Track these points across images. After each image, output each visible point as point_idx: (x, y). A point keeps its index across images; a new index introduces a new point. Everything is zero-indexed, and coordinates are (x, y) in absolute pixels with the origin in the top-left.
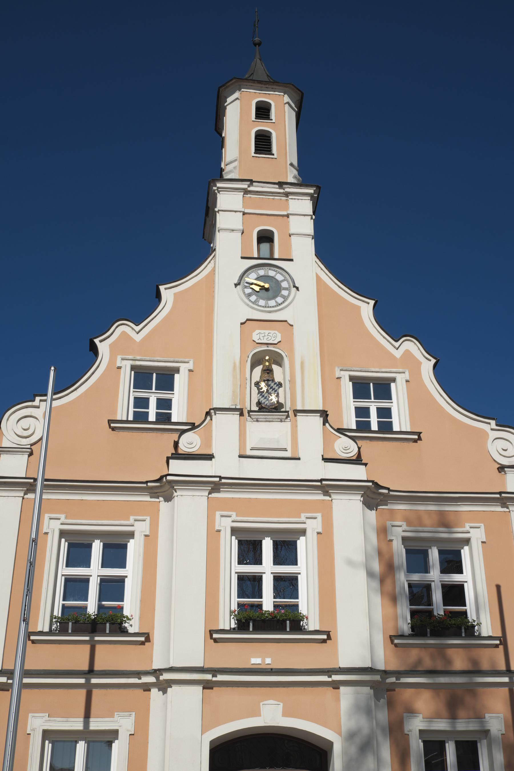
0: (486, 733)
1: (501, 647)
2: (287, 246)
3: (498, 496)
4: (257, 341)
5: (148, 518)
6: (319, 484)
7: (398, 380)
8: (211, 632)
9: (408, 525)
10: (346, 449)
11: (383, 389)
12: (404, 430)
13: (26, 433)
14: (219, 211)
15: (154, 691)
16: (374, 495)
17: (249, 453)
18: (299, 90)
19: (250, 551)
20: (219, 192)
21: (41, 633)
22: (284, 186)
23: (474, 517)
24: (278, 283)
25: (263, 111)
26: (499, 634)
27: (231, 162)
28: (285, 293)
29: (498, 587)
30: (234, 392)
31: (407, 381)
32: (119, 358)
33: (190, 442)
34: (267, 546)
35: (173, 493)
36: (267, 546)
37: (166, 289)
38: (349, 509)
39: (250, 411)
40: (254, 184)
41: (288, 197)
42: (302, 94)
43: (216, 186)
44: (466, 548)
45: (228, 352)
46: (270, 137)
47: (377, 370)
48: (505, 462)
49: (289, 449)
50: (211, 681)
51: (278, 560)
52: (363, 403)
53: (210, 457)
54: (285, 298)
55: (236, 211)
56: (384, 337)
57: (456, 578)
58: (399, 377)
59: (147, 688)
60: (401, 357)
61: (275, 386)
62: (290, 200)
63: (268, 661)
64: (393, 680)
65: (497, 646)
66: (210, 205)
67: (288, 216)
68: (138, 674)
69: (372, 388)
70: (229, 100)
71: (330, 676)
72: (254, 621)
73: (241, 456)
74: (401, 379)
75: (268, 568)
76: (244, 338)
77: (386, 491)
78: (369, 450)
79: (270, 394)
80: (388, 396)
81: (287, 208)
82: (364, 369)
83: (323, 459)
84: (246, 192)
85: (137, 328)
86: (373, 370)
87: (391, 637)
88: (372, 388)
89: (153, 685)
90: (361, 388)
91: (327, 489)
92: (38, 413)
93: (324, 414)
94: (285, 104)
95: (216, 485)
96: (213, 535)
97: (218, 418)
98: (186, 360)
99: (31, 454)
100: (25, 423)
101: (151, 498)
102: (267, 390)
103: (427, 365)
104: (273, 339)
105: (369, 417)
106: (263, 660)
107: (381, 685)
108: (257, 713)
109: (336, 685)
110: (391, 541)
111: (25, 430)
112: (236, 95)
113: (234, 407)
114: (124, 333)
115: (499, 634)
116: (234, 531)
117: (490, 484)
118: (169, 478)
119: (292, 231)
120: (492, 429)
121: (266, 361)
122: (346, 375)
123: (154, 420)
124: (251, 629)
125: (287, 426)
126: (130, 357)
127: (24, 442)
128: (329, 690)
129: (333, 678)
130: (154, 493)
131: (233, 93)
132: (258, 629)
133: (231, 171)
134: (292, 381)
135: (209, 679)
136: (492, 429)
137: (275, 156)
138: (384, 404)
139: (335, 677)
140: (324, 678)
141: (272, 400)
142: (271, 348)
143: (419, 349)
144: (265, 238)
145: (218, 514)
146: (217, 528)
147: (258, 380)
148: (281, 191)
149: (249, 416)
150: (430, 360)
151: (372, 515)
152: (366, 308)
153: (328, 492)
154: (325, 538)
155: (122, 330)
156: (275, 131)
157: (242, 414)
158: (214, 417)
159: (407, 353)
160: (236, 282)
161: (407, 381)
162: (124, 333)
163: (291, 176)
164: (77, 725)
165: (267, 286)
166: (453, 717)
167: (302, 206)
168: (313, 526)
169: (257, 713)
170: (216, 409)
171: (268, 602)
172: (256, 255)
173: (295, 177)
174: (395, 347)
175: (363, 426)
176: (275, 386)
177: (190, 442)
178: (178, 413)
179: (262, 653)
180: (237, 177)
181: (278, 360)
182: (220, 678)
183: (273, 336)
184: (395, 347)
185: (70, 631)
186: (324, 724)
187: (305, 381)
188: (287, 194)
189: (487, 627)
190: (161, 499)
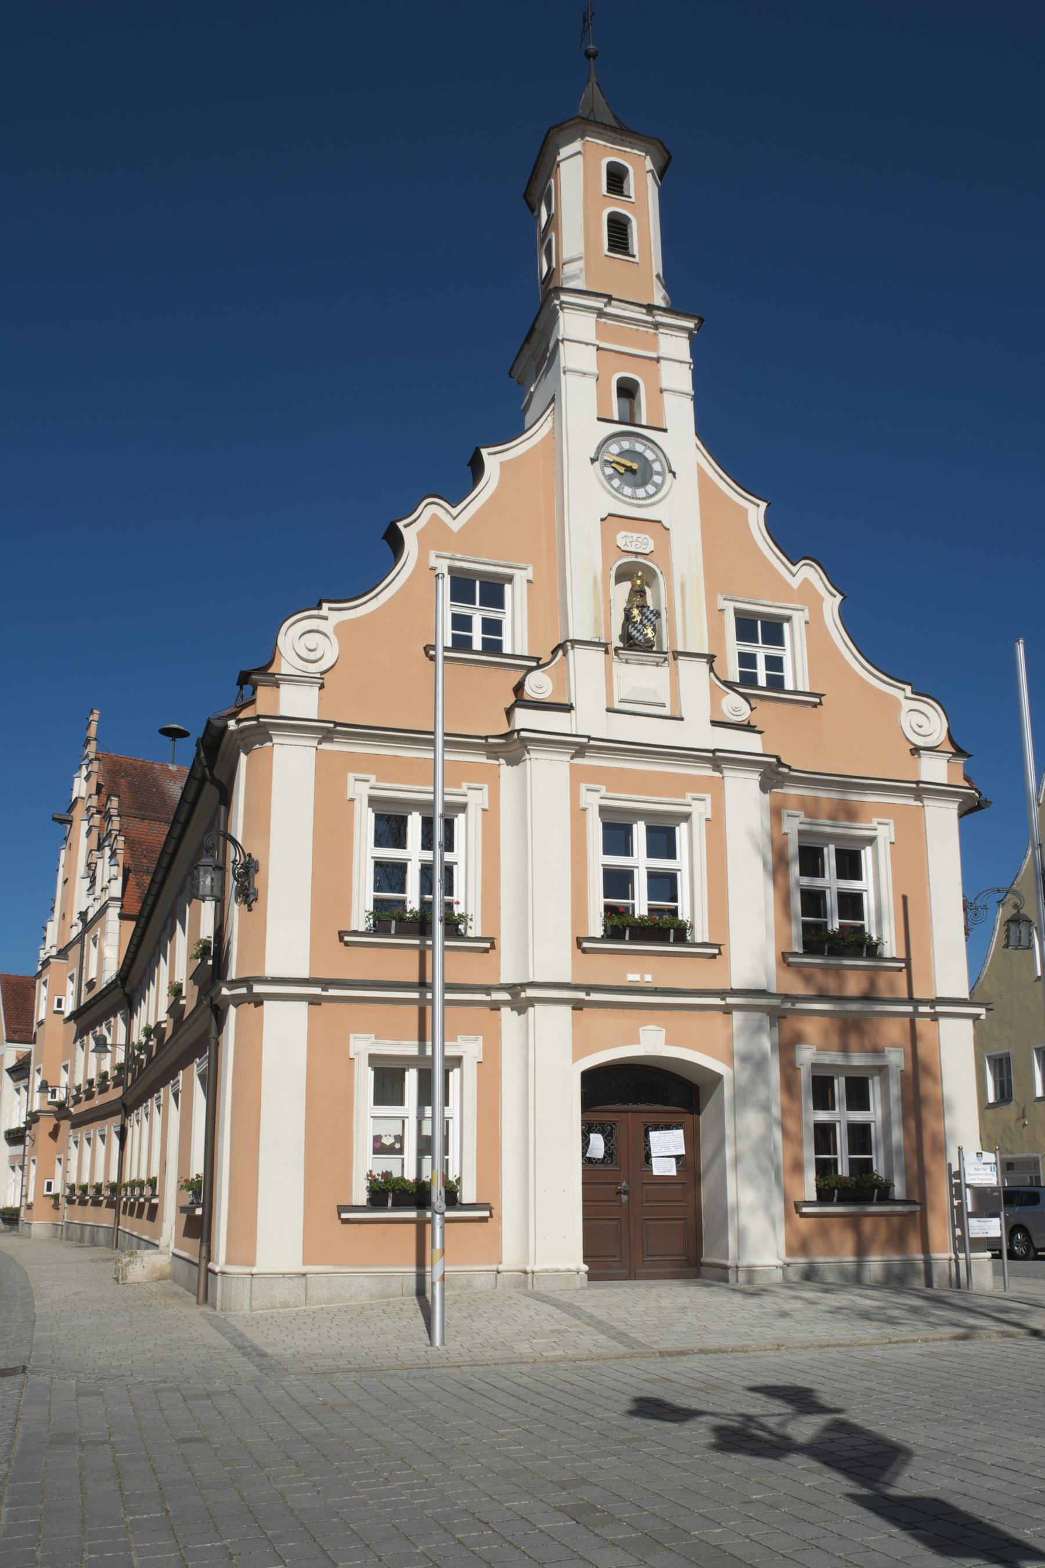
0: (882, 1070)
1: (904, 970)
2: (657, 407)
3: (914, 786)
5: (486, 787)
6: (710, 755)
7: (517, 580)
9: (806, 816)
10: (736, 709)
11: (773, 632)
13: (312, 656)
14: (564, 340)
15: (505, 1011)
16: (773, 774)
17: (617, 706)
18: (667, 151)
19: (617, 838)
20: (562, 309)
21: (355, 933)
22: (655, 312)
23: (884, 811)
24: (646, 463)
25: (616, 179)
26: (903, 956)
27: (573, 260)
28: (657, 479)
29: (905, 898)
30: (596, 619)
31: (529, 582)
32: (432, 554)
33: (539, 685)
34: (639, 832)
35: (524, 755)
36: (639, 832)
37: (489, 454)
38: (743, 791)
39: (617, 649)
40: (613, 302)
41: (657, 329)
42: (670, 158)
43: (558, 298)
44: (869, 849)
45: (585, 559)
46: (626, 226)
47: (770, 603)
48: (920, 742)
49: (668, 705)
50: (583, 1000)
52: (748, 648)
53: (568, 708)
54: (659, 487)
55: (587, 344)
56: (778, 557)
57: (853, 885)
58: (796, 616)
59: (496, 1006)
60: (800, 587)
61: (651, 616)
62: (660, 335)
63: (648, 978)
64: (788, 1005)
65: (900, 969)
66: (539, 326)
67: (658, 360)
68: (488, 989)
69: (761, 628)
70: (564, 152)
71: (723, 999)
72: (632, 928)
73: (608, 710)
74: (799, 618)
75: (640, 861)
76: (607, 540)
77: (786, 770)
78: (767, 714)
79: (645, 626)
80: (499, 603)
81: (655, 347)
82: (753, 601)
83: (712, 722)
84: (601, 314)
85: (454, 511)
86: (765, 602)
87: (783, 954)
88: (761, 628)
89: (505, 1003)
91: (719, 762)
92: (327, 627)
93: (711, 659)
94: (648, 172)
95: (581, 747)
96: (578, 814)
97: (578, 656)
98: (523, 565)
99: (322, 687)
100: (312, 640)
101: (488, 758)
103: (831, 603)
104: (644, 546)
105: (483, 639)
106: (642, 977)
107: (775, 1010)
108: (635, 1040)
109: (727, 1010)
111: (310, 650)
112: (576, 146)
113: (597, 640)
114: (435, 516)
115: (903, 956)
116: (373, 801)
117: (900, 769)
118: (523, 734)
119: (664, 386)
120: (906, 698)
121: (636, 575)
122: (730, 607)
123: (480, 649)
124: (627, 938)
125: (664, 672)
126: (448, 554)
127: (313, 668)
128: (719, 1016)
129: (727, 1000)
130: (493, 752)
131: (571, 141)
132: (635, 938)
133: (575, 277)
134: (671, 610)
135: (581, 998)
136: (906, 698)
138: (492, 614)
139: (730, 1000)
140: (717, 1001)
141: (646, 634)
142: (640, 560)
143: (821, 578)
144: (627, 390)
145: (583, 786)
146: (350, 796)
148: (649, 319)
149: (617, 654)
150: (835, 596)
151: (767, 797)
152: (756, 512)
153: (719, 766)
154: (716, 825)
155: (431, 511)
156: (635, 217)
157: (607, 652)
158: (570, 652)
159: (806, 582)
162: (435, 516)
163: (659, 297)
164: (411, 1048)
165: (635, 466)
166: (845, 1049)
167: (675, 346)
168: (701, 811)
169: (635, 1040)
170: (575, 642)
171: (641, 904)
173: (664, 298)
174: (791, 572)
175: (748, 680)
176: (651, 616)
177: (539, 685)
179: (641, 968)
180: (583, 287)
181: (650, 576)
182: (595, 997)
183: (640, 542)
184: (791, 572)
185: (393, 932)
187: (692, 614)
188: (657, 326)
189: (891, 947)
190: (502, 761)
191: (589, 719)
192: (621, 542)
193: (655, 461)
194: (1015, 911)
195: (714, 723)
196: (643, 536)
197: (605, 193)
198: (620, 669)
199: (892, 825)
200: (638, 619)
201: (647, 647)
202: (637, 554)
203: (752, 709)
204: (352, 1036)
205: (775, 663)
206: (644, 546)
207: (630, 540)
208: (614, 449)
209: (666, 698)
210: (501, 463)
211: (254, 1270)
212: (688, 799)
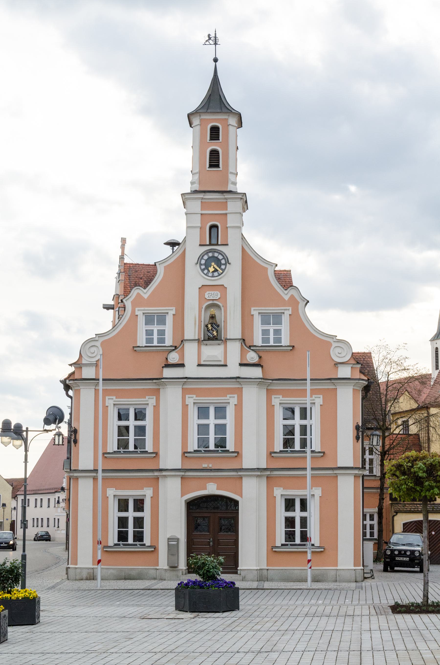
4: (207, 299)
8: (184, 453)
10: (252, 358)
13: (93, 355)
17: (202, 363)
21: (109, 453)
33: (174, 358)
49: (223, 360)
52: (266, 327)
63: (210, 466)
75: (212, 421)
96: (185, 407)
100: (93, 349)
102: (212, 329)
110: (188, 405)
114: (138, 294)
125: (222, 347)
147: (207, 323)
160: (196, 262)
161: (290, 315)
162: (138, 294)
168: (233, 400)
170: (185, 340)
172: (208, 243)
178: (169, 341)
183: (215, 295)
186: (235, 493)
191: (191, 370)
192: (206, 296)
193: (222, 259)
197: (208, 141)
198: (203, 348)
200: (210, 328)
201: (215, 338)
202: (213, 300)
206: (216, 296)
208: (206, 257)
210: (164, 267)
211: (338, 568)
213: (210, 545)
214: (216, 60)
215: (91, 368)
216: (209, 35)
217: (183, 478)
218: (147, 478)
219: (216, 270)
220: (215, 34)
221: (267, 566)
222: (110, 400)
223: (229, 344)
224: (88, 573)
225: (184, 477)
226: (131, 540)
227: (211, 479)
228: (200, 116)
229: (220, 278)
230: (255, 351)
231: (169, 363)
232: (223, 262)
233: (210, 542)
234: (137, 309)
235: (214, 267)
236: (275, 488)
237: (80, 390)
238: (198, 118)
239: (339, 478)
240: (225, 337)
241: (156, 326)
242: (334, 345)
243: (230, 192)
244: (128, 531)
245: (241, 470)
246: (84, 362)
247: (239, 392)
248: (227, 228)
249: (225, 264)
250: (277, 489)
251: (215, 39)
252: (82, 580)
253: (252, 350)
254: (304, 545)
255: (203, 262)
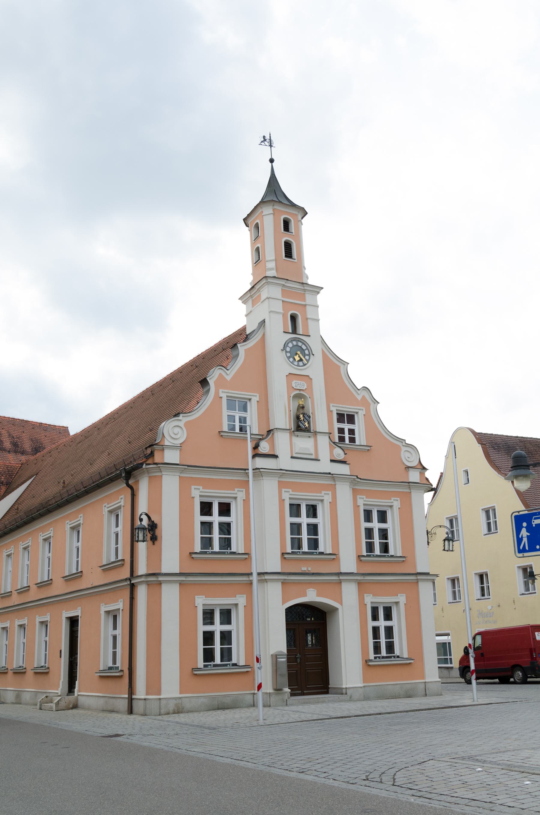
10: (339, 455)
11: (351, 419)
12: (362, 444)
17: (295, 455)
21: (196, 553)
33: (264, 447)
38: (344, 492)
51: (221, 514)
52: (341, 426)
58: (360, 412)
73: (292, 457)
74: (361, 413)
76: (290, 387)
90: (341, 418)
95: (282, 473)
100: (177, 430)
108: (305, 595)
110: (284, 500)
114: (220, 374)
118: (261, 470)
125: (312, 440)
133: (271, 269)
137: (296, 261)
142: (301, 392)
144: (293, 318)
145: (283, 490)
154: (333, 504)
160: (282, 348)
162: (220, 374)
168: (328, 499)
169: (305, 595)
191: (284, 462)
192: (294, 385)
194: (447, 536)
195: (332, 461)
196: (302, 382)
198: (294, 439)
199: (399, 501)
200: (302, 419)
201: (307, 430)
202: (300, 390)
203: (345, 454)
204: (196, 597)
205: (352, 432)
207: (297, 384)
208: (290, 345)
209: (312, 451)
210: (245, 350)
211: (161, 697)
212: (323, 494)
213: (296, 662)
214: (272, 161)
215: (174, 451)
216: (264, 137)
217: (284, 583)
218: (239, 583)
219: (301, 360)
220: (270, 137)
221: (180, 694)
222: (196, 490)
223: (319, 437)
224: (176, 705)
225: (285, 581)
226: (218, 660)
227: (311, 584)
228: (273, 205)
229: (306, 369)
230: (343, 450)
231: (260, 453)
232: (307, 352)
233: (297, 658)
234: (221, 390)
235: (299, 357)
236: (365, 595)
237: (161, 476)
238: (271, 207)
239: (420, 584)
240: (315, 430)
241: (237, 412)
242: (404, 449)
243: (306, 284)
244: (231, 648)
245: (340, 574)
246: (167, 443)
247: (333, 488)
248: (307, 319)
249: (309, 355)
250: (367, 596)
251: (270, 142)
252: (168, 714)
253: (340, 447)
254: (390, 657)
255: (288, 349)
